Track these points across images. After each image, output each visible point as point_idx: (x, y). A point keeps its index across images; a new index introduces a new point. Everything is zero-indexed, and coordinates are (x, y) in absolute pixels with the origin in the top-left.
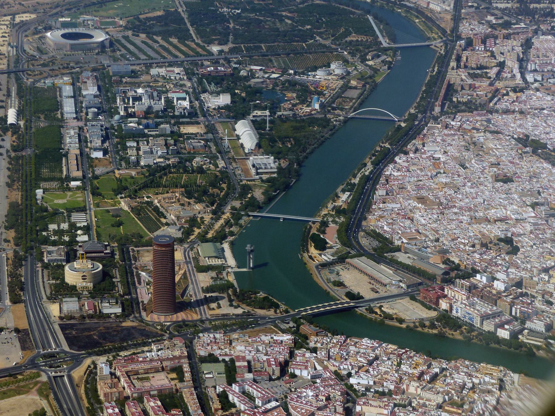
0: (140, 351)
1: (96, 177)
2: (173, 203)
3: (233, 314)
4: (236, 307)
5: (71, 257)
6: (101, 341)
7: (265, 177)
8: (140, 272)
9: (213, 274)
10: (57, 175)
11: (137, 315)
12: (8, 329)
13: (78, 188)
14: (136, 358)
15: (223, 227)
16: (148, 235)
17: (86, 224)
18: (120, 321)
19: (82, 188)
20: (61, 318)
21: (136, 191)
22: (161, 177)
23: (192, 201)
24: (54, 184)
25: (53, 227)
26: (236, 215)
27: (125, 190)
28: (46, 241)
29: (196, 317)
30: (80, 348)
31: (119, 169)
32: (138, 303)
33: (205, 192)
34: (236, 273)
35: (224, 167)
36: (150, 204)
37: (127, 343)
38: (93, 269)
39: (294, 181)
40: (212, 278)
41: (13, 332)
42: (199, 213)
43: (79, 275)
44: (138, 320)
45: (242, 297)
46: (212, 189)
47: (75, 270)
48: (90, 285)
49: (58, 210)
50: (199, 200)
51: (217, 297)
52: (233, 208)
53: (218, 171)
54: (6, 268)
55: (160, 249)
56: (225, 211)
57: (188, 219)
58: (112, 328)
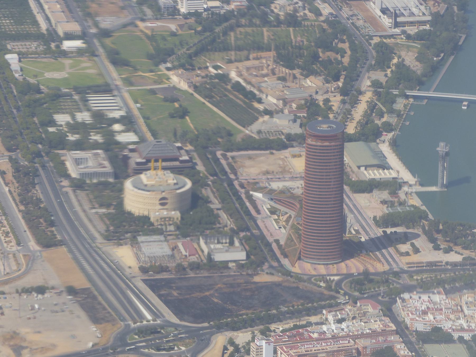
0: (304, 323)
1: (106, 33)
2: (264, 76)
3: (447, 263)
4: (447, 251)
5: (122, 168)
6: (229, 307)
7: (412, 30)
8: (251, 192)
9: (385, 195)
10: (33, 30)
11: (275, 264)
12: (53, 288)
13: (80, 52)
14: (306, 333)
15: (367, 115)
16: (241, 132)
17: (122, 113)
18: (248, 274)
19: (90, 52)
20: (144, 270)
21: (190, 57)
22: (225, 33)
23: (297, 72)
24: (33, 46)
25: (62, 119)
26: (383, 94)
27: (170, 56)
28: (60, 142)
29: (381, 267)
30: (197, 318)
31: (143, 20)
32: (268, 245)
33: (315, 57)
34: (420, 195)
35: (331, 14)
36: (224, 78)
37: (277, 309)
38: (177, 187)
39: (464, 36)
40: (384, 202)
41: (64, 294)
42: (317, 93)
43: (154, 198)
44: (279, 271)
45: (447, 232)
46: (323, 53)
47: (145, 188)
48: (176, 215)
49: (60, 90)
50: (309, 72)
51: (405, 233)
52: (376, 84)
53: (324, 22)
54: (7, 189)
55: (319, 144)
56: (363, 89)
57: (303, 102)
58: (239, 285)
